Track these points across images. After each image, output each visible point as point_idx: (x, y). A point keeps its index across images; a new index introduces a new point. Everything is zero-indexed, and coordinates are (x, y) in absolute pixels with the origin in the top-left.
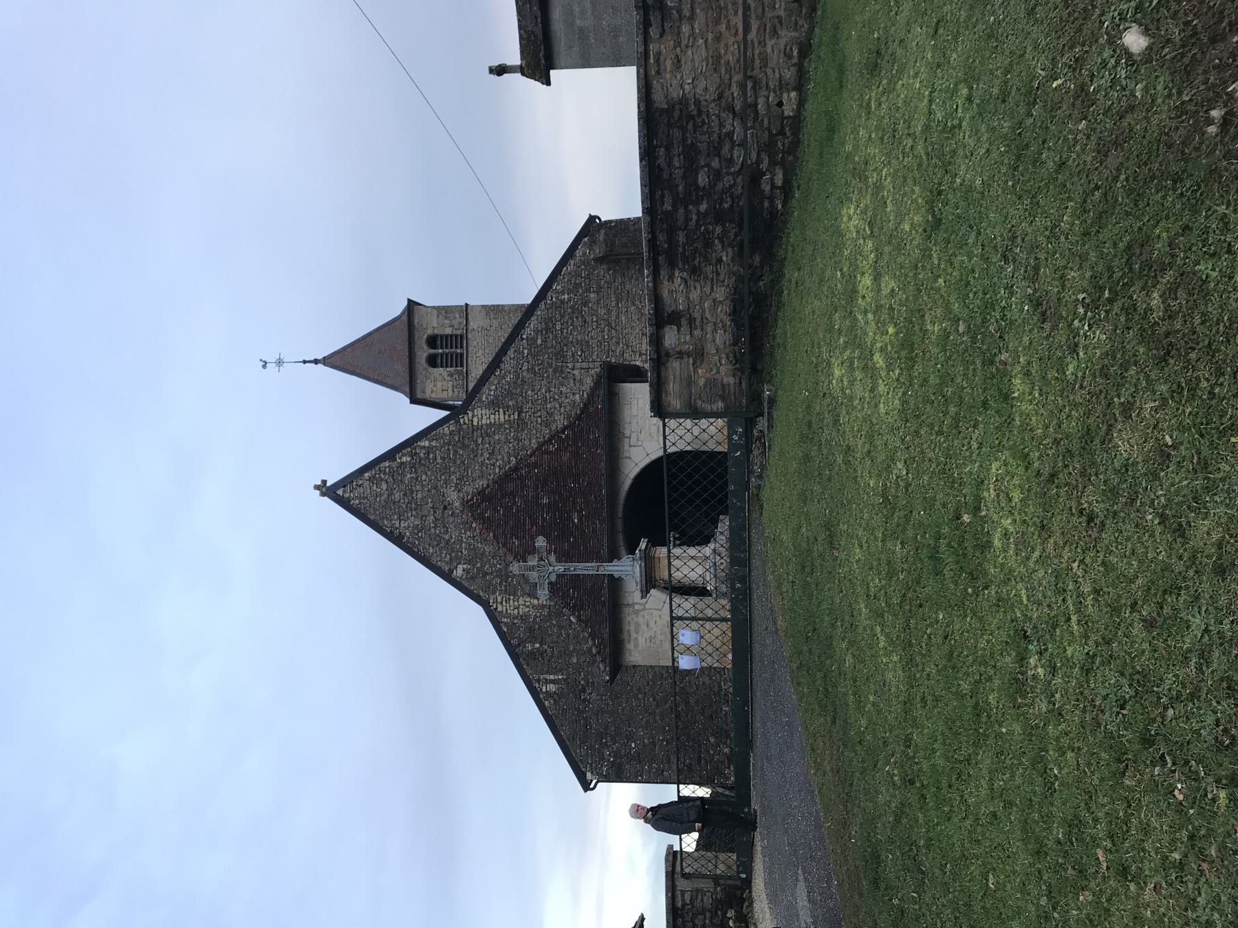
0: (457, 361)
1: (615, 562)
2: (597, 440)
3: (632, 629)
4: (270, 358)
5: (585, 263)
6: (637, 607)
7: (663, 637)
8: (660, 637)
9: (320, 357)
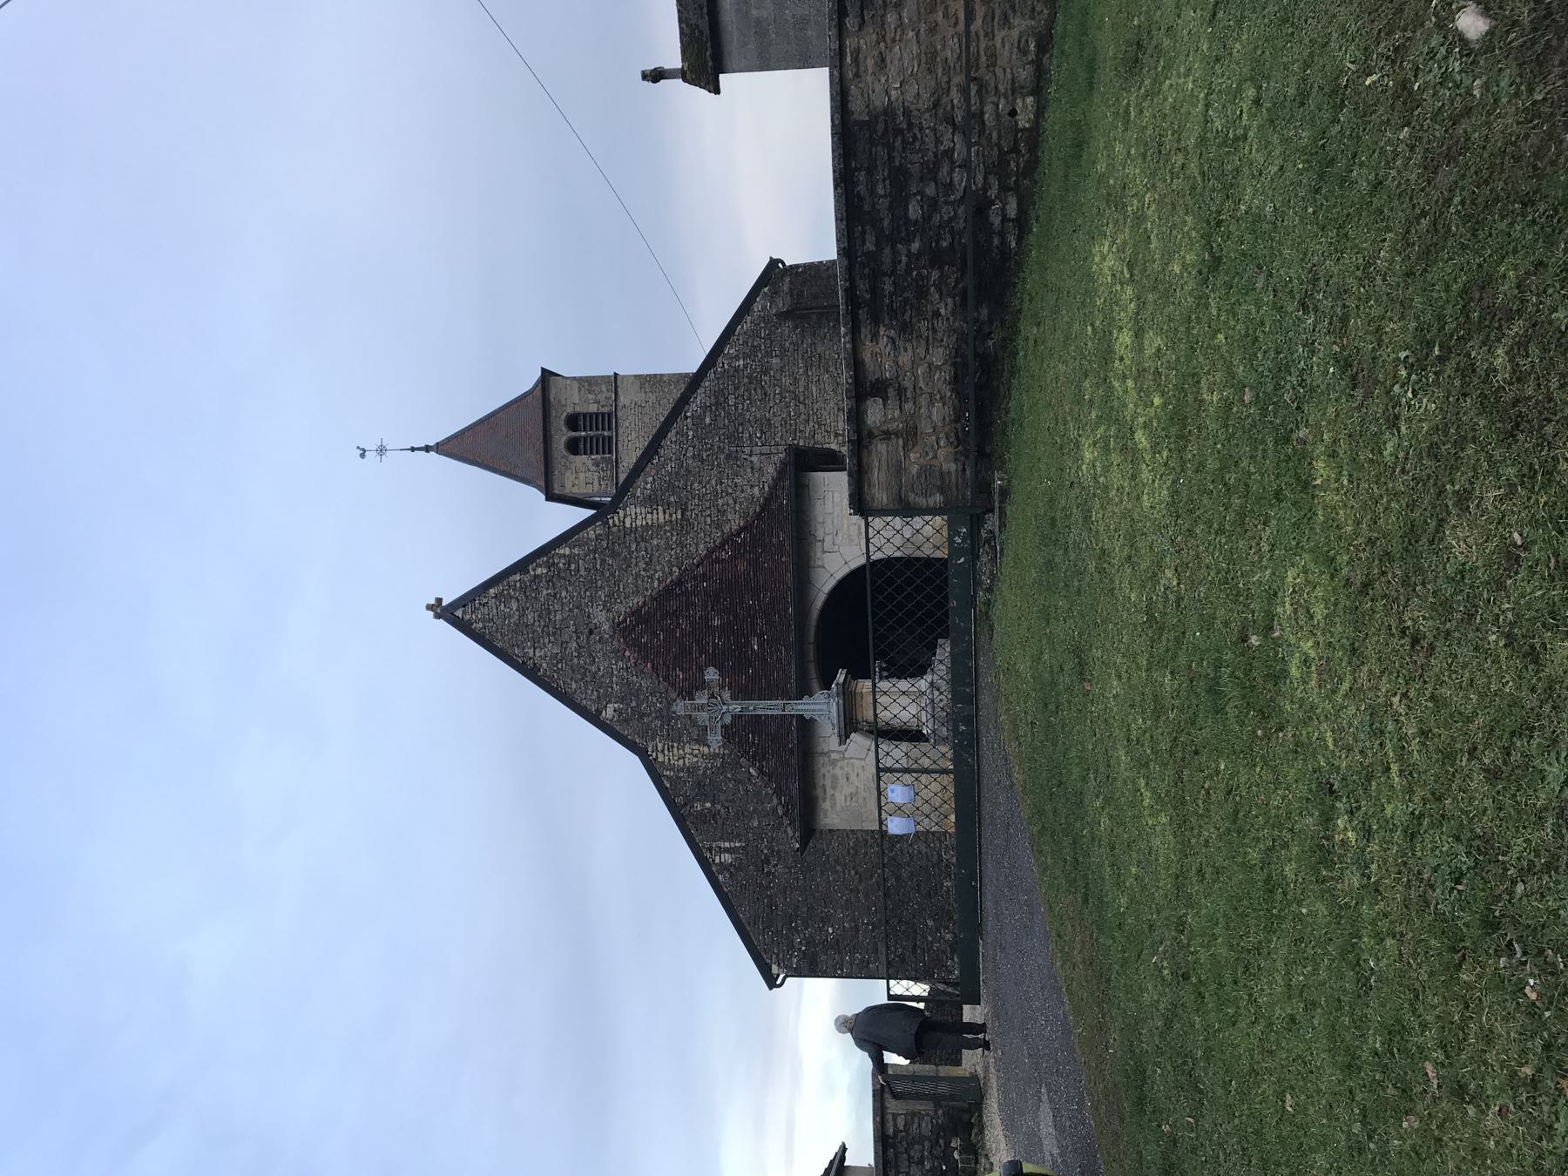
0: (606, 446)
1: (806, 699)
3: (828, 783)
4: (370, 445)
5: (765, 319)
6: (833, 756)
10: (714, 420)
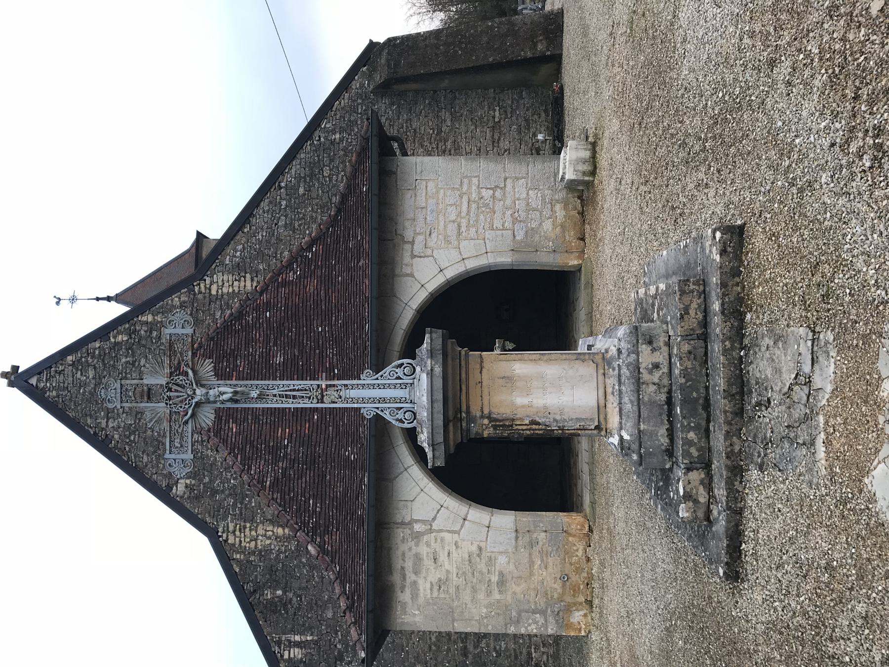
1: (367, 377)
2: (359, 245)
3: (409, 565)
4: (65, 295)
5: (364, 97)
6: (417, 527)
7: (461, 581)
8: (456, 581)
9: (112, 294)
10: (308, 190)
